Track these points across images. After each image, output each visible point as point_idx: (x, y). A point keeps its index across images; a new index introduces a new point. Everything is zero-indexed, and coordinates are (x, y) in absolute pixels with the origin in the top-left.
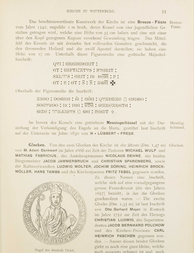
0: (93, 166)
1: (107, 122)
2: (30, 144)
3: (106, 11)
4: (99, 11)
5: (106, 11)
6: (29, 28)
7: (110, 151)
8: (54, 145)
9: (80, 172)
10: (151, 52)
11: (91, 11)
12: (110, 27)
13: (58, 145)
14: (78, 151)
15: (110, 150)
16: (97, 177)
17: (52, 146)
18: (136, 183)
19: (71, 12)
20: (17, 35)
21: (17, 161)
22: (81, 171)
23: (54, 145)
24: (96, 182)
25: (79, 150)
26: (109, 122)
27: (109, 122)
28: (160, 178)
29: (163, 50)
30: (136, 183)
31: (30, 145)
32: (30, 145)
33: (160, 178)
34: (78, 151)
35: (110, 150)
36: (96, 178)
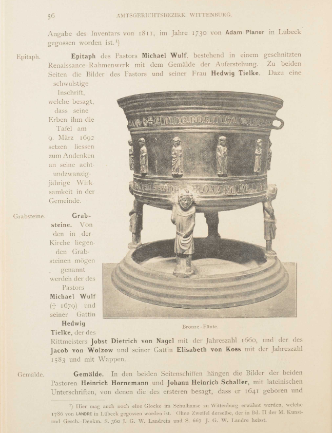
0: (250, 381)
1: (51, 295)
2: (76, 373)
3: (217, 15)
4: (205, 15)
5: (217, 15)
6: (178, 34)
7: (55, 384)
8: (87, 225)
9: (55, 244)
10: (79, 178)
11: (192, 15)
12: (85, 145)
13: (83, 120)
14: (246, 340)
15: (53, 382)
16: (271, 64)
17: (84, 226)
18: (103, 393)
19: (177, 16)
20: (91, 143)
21: (248, 374)
22: (57, 242)
23: (87, 225)
24: (173, 52)
25: (248, 339)
26: (54, 295)
27: (54, 295)
28: (81, 393)
29: (62, 261)
30: (103, 393)
31: (76, 375)
32: (76, 375)
33: (81, 393)
34: (246, 340)
35: (53, 382)
36: (270, 64)
